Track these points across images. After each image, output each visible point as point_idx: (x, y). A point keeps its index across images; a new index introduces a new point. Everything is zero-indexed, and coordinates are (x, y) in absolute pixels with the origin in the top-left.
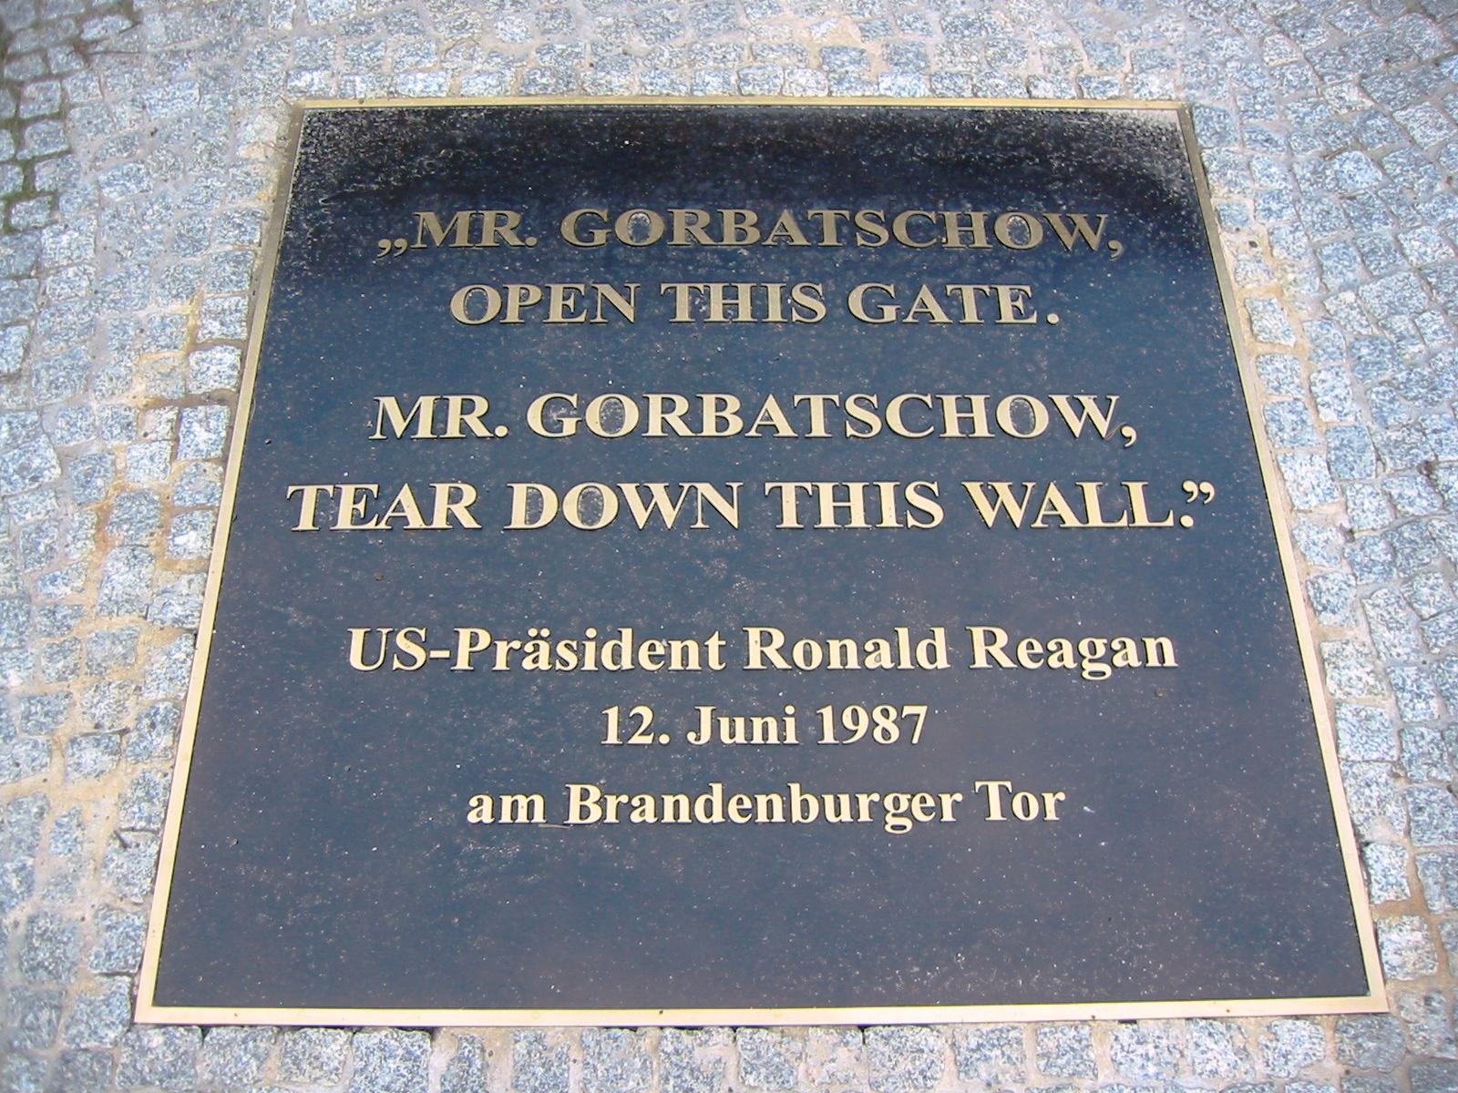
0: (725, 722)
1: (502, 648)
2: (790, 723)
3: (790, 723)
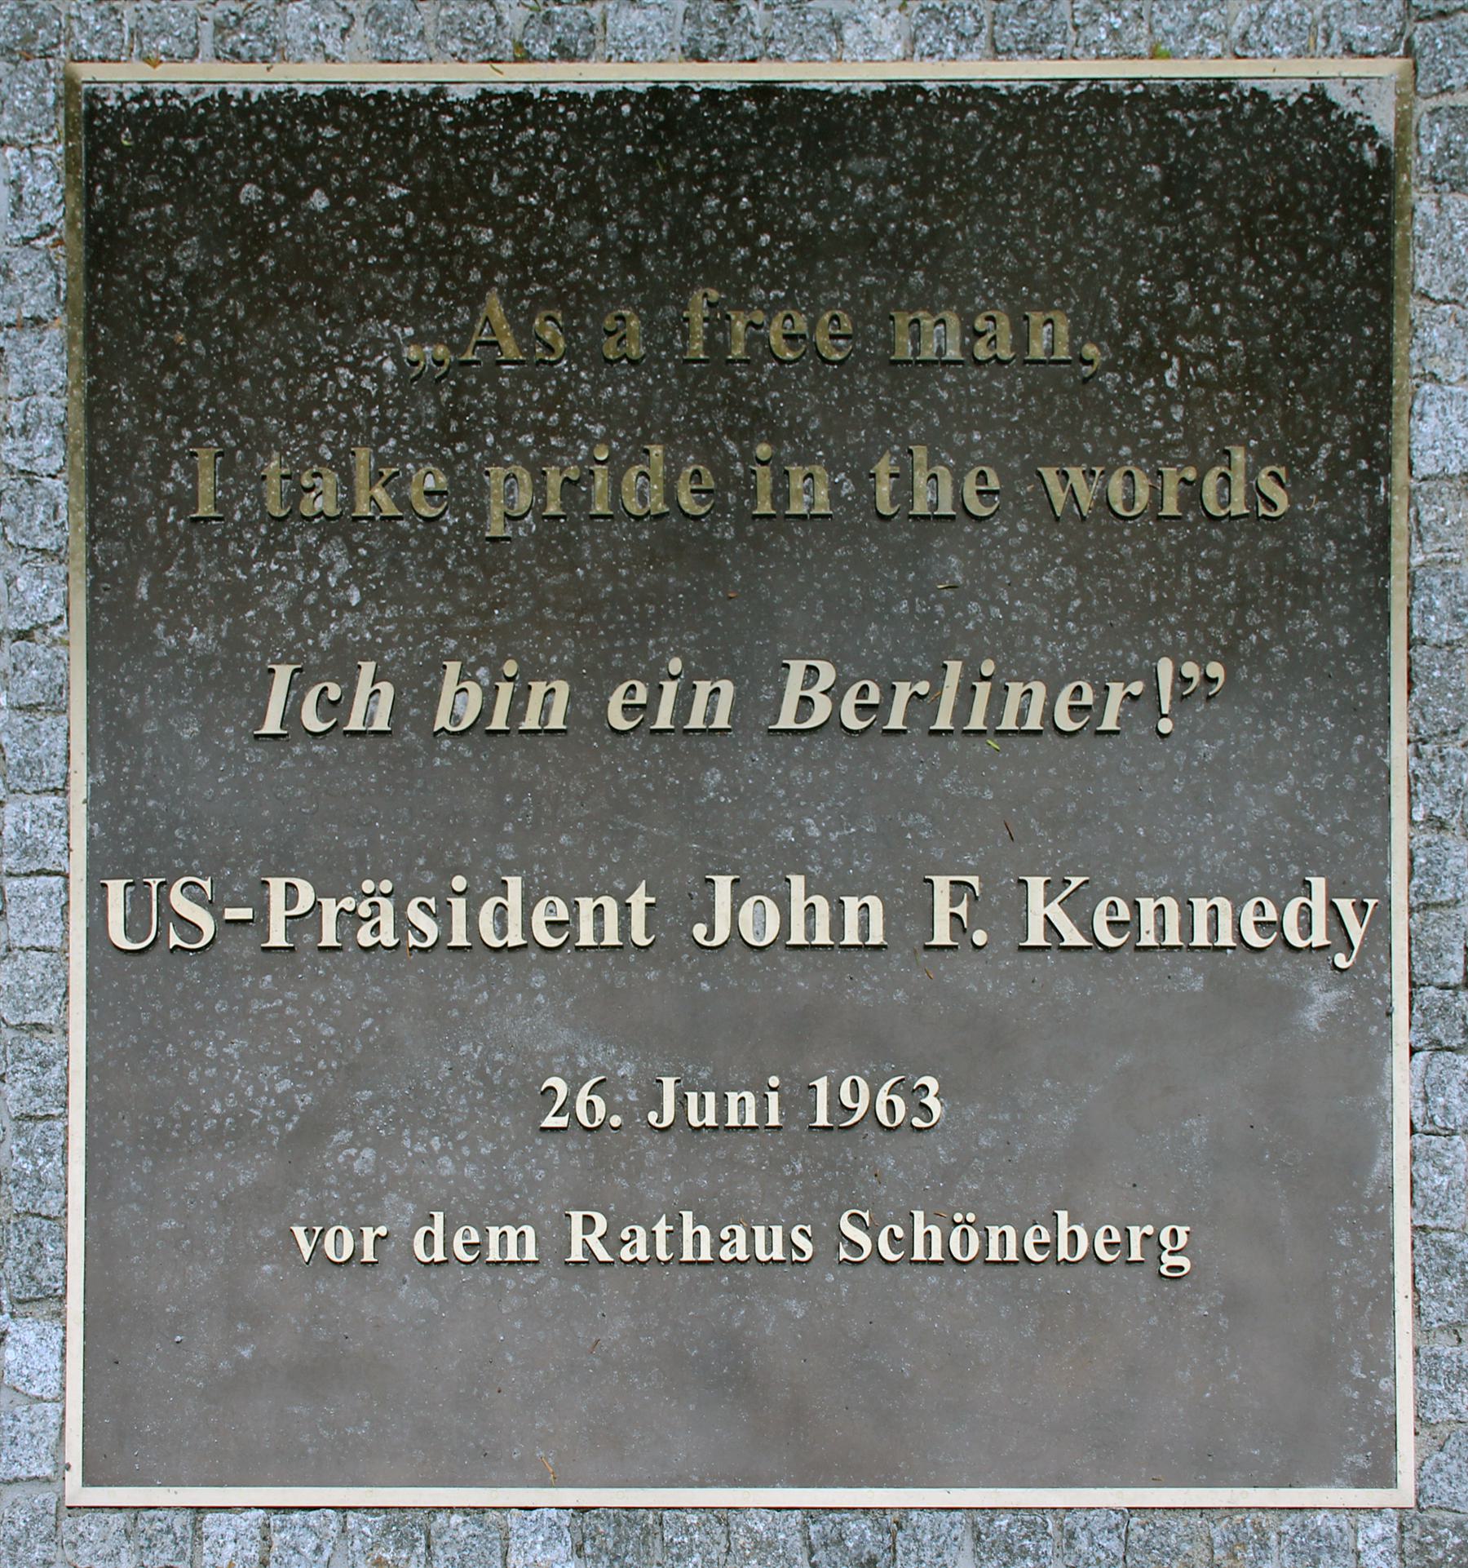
0: (693, 1097)
1: (330, 908)
2: (773, 1097)
3: (773, 1097)
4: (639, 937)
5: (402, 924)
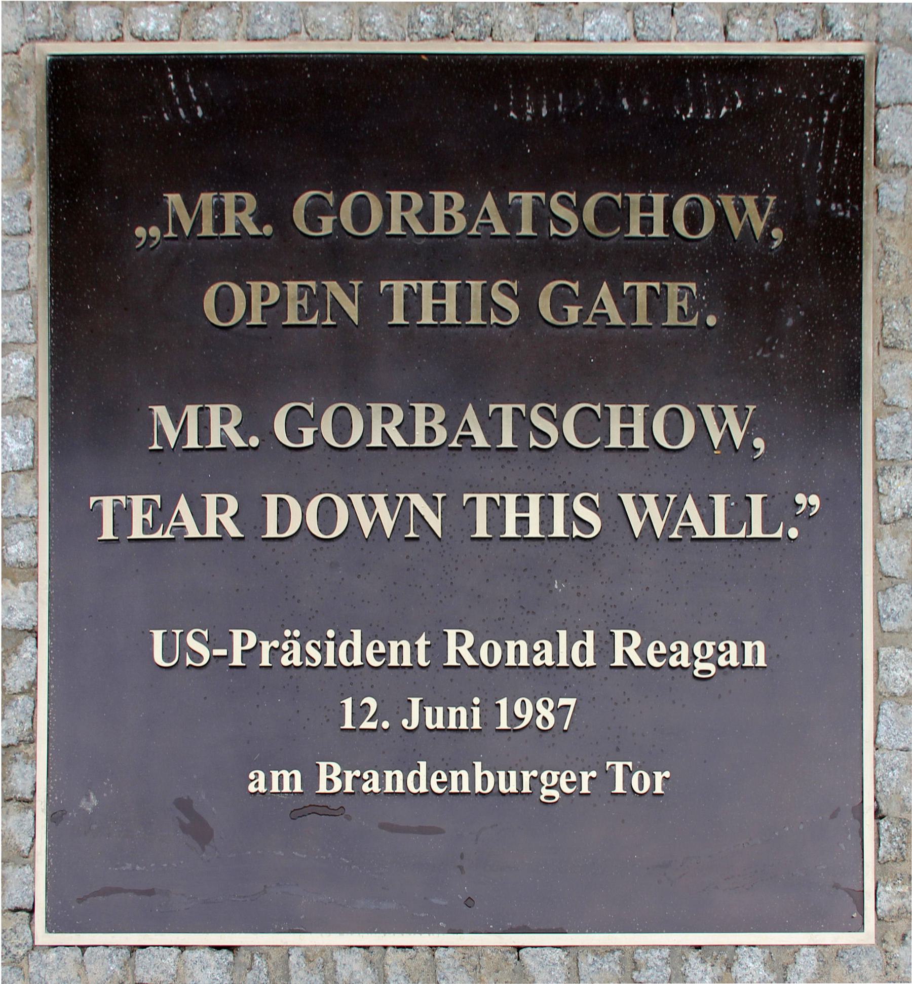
0: (429, 710)
1: (266, 646)
2: (476, 711)
3: (476, 711)
4: (422, 662)
5: (304, 654)
